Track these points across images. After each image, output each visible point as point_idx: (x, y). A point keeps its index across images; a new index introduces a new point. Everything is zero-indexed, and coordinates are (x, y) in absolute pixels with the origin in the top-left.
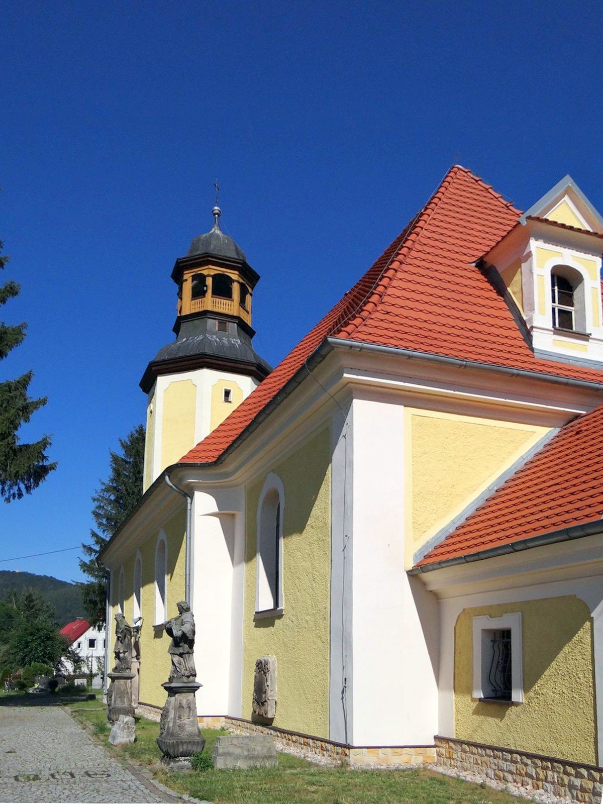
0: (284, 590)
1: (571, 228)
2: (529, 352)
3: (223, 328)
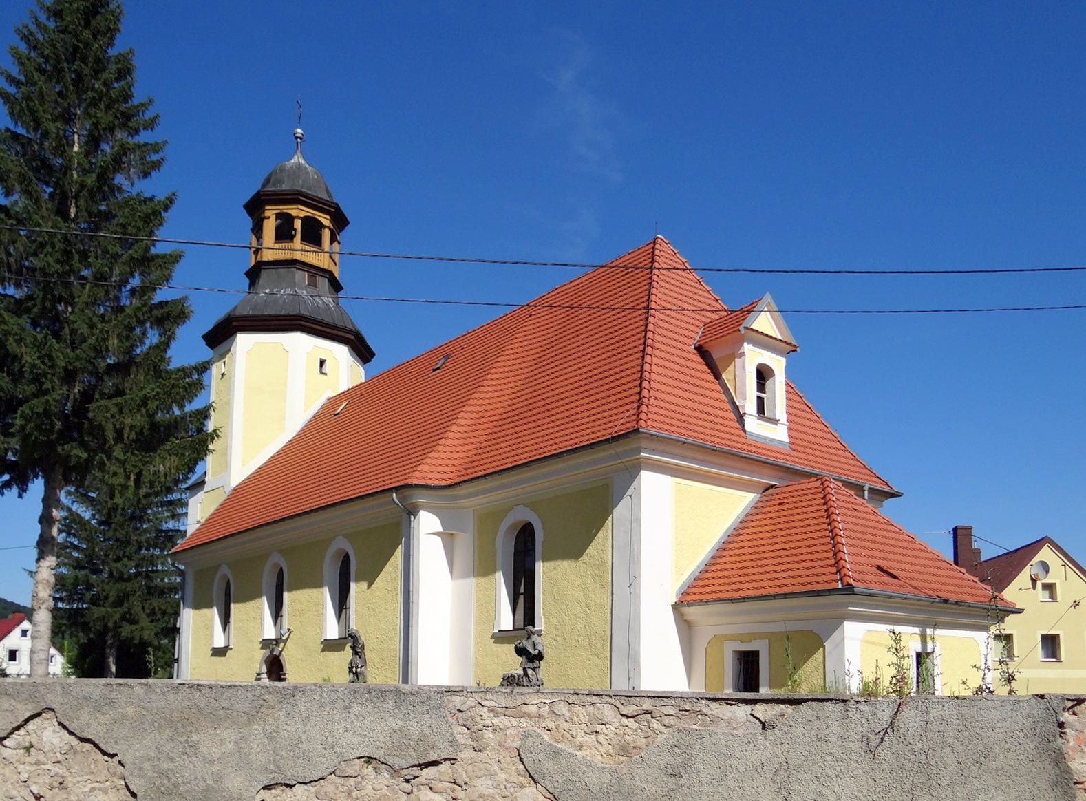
0: (544, 613)
1: (771, 337)
2: (743, 434)
3: (313, 284)
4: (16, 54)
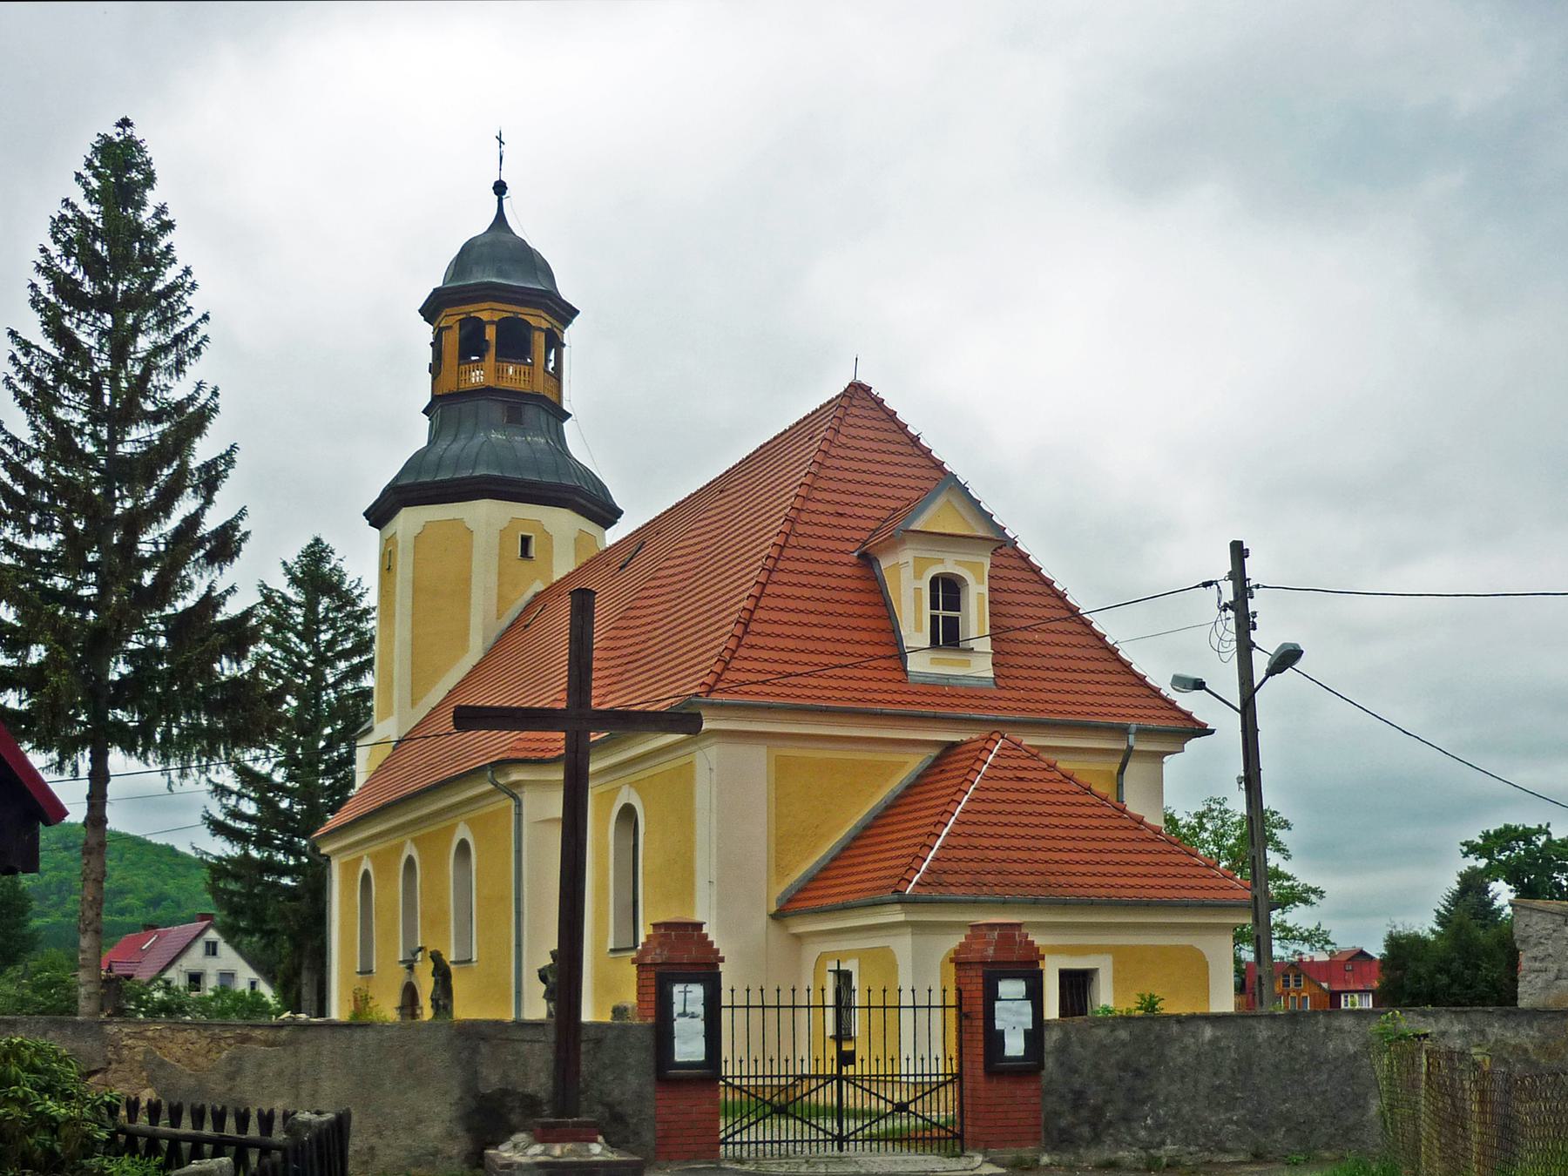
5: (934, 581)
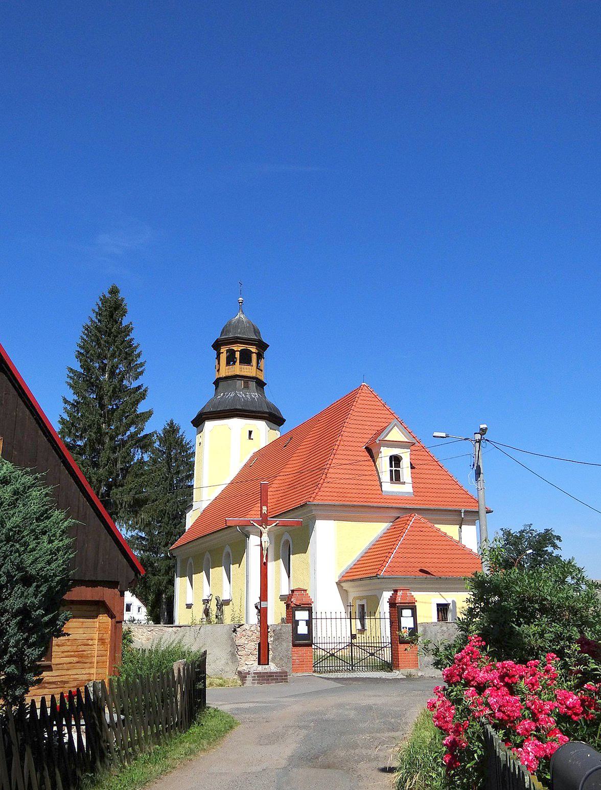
3: (246, 386)
4: (83, 339)
5: (391, 457)
